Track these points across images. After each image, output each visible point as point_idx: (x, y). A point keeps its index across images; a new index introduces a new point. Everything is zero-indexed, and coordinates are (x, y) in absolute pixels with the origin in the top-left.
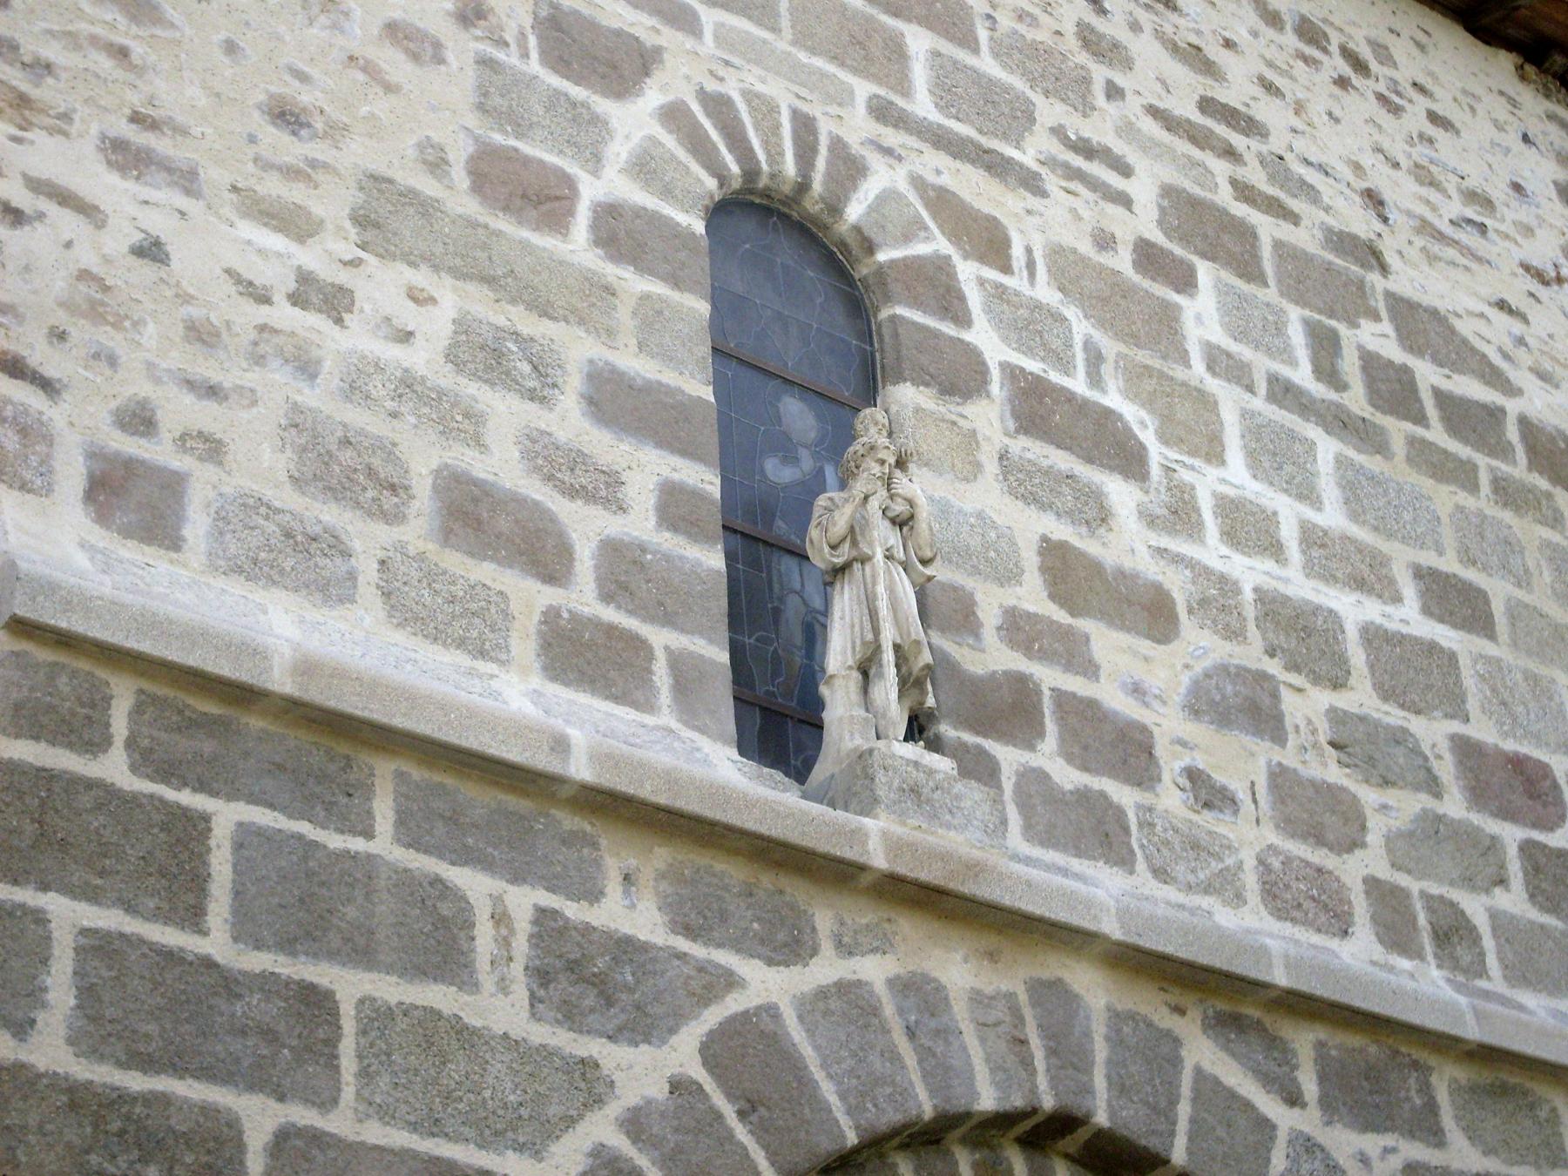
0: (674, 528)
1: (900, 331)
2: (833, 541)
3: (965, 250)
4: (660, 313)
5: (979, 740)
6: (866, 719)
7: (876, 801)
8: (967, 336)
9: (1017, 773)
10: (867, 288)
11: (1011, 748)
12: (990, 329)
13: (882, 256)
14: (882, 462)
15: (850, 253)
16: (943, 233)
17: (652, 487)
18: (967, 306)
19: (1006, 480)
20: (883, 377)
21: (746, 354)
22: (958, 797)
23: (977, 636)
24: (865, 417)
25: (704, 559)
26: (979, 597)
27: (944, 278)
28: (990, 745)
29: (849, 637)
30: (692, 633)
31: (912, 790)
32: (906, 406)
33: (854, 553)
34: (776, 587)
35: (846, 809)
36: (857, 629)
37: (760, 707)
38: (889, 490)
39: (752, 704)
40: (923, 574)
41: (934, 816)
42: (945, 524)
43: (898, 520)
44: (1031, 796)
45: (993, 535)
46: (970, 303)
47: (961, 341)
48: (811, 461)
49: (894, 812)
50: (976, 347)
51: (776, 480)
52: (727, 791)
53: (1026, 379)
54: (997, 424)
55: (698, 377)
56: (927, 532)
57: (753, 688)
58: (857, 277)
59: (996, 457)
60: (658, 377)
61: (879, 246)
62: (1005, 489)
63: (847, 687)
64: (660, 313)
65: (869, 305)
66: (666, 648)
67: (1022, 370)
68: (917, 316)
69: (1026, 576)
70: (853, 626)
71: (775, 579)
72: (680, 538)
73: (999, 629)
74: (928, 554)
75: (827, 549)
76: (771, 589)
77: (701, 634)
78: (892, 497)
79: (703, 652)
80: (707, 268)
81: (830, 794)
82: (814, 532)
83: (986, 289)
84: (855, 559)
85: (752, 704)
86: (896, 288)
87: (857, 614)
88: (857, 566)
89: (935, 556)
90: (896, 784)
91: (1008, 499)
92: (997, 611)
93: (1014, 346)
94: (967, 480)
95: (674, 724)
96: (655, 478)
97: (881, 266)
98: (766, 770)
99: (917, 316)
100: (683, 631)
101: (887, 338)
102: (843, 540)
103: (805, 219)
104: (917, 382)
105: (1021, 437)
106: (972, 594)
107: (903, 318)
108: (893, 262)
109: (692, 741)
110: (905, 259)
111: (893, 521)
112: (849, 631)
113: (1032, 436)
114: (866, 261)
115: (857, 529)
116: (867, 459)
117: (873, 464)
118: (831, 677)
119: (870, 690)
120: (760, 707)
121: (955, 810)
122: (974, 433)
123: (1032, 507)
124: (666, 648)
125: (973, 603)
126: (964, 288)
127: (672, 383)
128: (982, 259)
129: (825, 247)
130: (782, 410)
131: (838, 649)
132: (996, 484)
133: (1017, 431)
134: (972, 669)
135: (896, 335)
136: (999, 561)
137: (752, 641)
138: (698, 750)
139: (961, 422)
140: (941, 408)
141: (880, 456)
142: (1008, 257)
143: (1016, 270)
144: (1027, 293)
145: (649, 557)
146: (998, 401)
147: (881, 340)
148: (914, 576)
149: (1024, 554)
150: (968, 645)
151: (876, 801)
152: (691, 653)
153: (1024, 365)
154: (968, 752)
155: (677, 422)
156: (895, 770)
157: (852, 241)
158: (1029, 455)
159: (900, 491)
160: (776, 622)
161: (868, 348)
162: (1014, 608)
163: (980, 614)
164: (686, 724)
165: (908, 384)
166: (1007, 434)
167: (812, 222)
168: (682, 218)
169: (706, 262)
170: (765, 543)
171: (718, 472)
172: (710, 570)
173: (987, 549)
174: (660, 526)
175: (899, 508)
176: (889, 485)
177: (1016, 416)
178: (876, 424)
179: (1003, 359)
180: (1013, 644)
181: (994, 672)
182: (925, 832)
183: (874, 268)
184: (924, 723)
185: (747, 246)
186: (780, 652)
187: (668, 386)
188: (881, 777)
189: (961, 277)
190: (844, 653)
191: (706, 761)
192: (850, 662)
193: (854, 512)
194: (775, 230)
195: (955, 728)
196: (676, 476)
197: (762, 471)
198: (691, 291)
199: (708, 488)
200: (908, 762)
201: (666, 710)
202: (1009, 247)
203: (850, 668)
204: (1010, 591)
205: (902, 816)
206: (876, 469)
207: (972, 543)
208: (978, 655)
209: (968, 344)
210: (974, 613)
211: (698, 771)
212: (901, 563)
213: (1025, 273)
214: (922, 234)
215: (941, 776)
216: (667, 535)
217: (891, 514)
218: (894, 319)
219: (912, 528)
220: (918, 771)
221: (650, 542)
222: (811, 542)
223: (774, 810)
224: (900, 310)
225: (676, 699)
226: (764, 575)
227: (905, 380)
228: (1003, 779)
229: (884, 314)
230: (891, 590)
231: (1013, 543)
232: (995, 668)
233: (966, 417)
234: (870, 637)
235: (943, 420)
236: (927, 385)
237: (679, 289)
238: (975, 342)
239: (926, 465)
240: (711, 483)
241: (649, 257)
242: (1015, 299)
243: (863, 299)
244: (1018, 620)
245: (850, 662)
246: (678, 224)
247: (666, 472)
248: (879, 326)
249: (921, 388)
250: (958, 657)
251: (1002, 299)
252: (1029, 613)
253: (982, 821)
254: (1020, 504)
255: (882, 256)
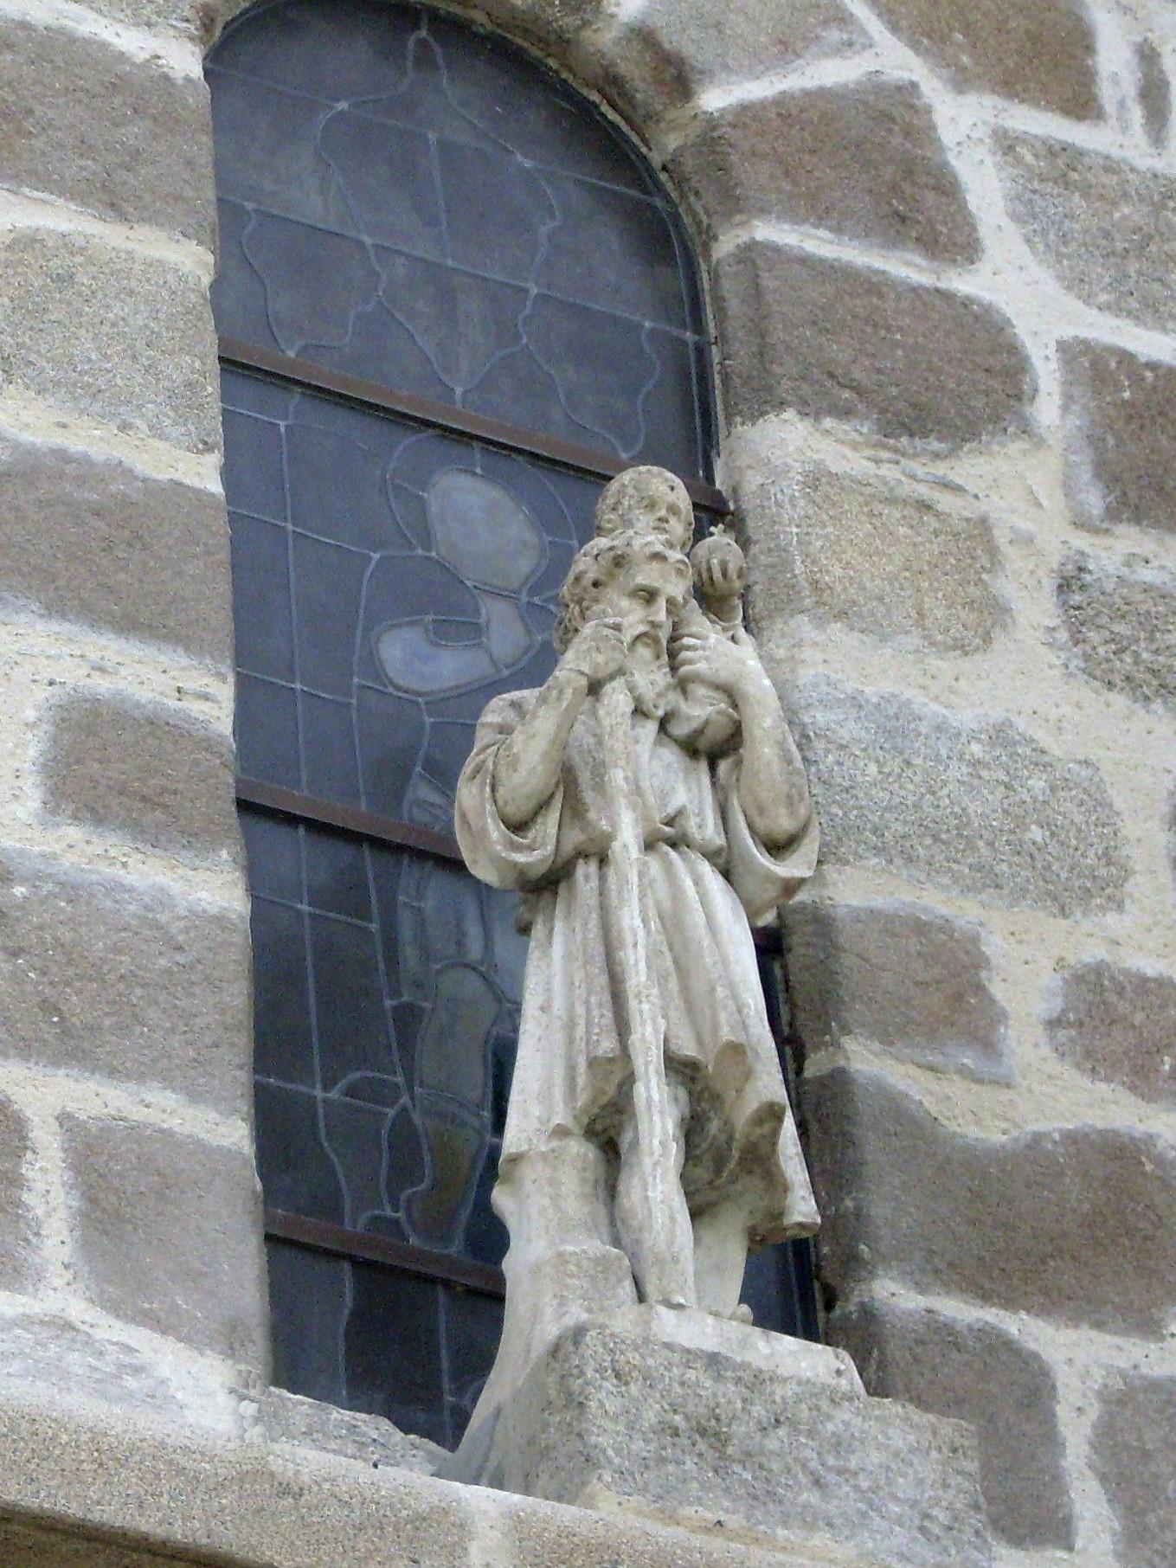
0: (94, 814)
1: (768, 281)
2: (515, 811)
3: (962, 69)
4: (65, 279)
5: (991, 1315)
6: (602, 1262)
7: (590, 1461)
8: (962, 283)
9: (1104, 1395)
10: (681, 182)
11: (1086, 1333)
12: (1029, 260)
13: (714, 99)
14: (649, 596)
15: (631, 100)
16: (894, 28)
17: (31, 714)
18: (963, 205)
19: (1077, 639)
20: (726, 405)
21: (326, 373)
22: (838, 1445)
23: (988, 1046)
24: (622, 491)
25: (176, 888)
26: (995, 945)
27: (896, 140)
28: (1019, 1326)
29: (560, 1051)
30: (141, 1078)
31: (703, 1432)
32: (779, 473)
33: (574, 837)
34: (410, 955)
35: (527, 1491)
36: (581, 1030)
37: (352, 1259)
38: (674, 669)
39: (328, 1253)
40: (769, 877)
41: (764, 1496)
42: (895, 765)
43: (703, 744)
44: (1146, 1455)
45: (1038, 784)
46: (973, 201)
47: (947, 296)
48: (518, 631)
49: (643, 1490)
50: (988, 309)
51: (414, 684)
52: (41, 1428)
53: (1137, 380)
54: (1053, 501)
55: (175, 432)
56: (776, 766)
57: (335, 1213)
58: (656, 159)
59: (1050, 584)
60: (58, 439)
61: (706, 74)
62: (1076, 663)
63: (553, 1182)
64: (65, 279)
65: (691, 230)
66: (64, 1119)
67: (1126, 357)
68: (818, 243)
69: (1137, 886)
70: (571, 1024)
71: (406, 932)
72: (112, 840)
73: (1053, 1024)
74: (783, 823)
75: (496, 832)
76: (393, 961)
77: (167, 1080)
78: (683, 686)
79: (173, 1123)
80: (204, 158)
81: (491, 1465)
82: (468, 794)
83: (1019, 161)
84: (582, 854)
85: (328, 1253)
86: (752, 175)
87: (580, 992)
88: (585, 873)
89: (805, 828)
90: (650, 1416)
91: (1086, 693)
92: (1050, 980)
93: (1103, 298)
94: (961, 647)
95: (78, 1309)
96: (42, 693)
97: (712, 122)
98: (338, 1414)
99: (818, 243)
100: (113, 1073)
101: (734, 306)
102: (543, 806)
103: (508, 29)
104: (810, 410)
105: (1121, 529)
106: (975, 940)
107: (777, 249)
108: (746, 113)
109: (130, 1350)
110: (781, 100)
111: (691, 748)
112: (559, 1037)
113: (1156, 524)
114: (672, 114)
115: (584, 778)
116: (610, 593)
117: (625, 603)
118: (515, 1159)
119: (621, 1187)
120: (352, 1259)
121: (831, 1478)
122: (984, 524)
123: (1157, 705)
124: (64, 1119)
125: (980, 962)
126: (953, 162)
127: (99, 453)
128: (1010, 86)
129: (569, 94)
130: (434, 508)
131: (535, 1086)
132: (1051, 657)
133: (1112, 515)
134: (973, 1132)
135: (756, 294)
136: (1053, 848)
137: (334, 1094)
138: (137, 1370)
139: (946, 502)
140: (888, 471)
141: (641, 580)
142: (1087, 78)
143: (1110, 108)
144: (1143, 163)
145: (19, 891)
146: (1055, 441)
147: (721, 313)
148: (750, 885)
149: (1130, 828)
150: (963, 1071)
151: (590, 1461)
152: (135, 1127)
153: (1131, 347)
154: (958, 1347)
155: (108, 549)
156: (648, 1378)
157: (633, 69)
158: (1147, 575)
159: (701, 667)
160: (407, 1042)
161: (689, 336)
162: (1099, 969)
163: (997, 989)
164: (115, 1308)
165: (790, 414)
166: (1081, 523)
167: (526, 32)
168: (132, 42)
169: (202, 149)
170: (379, 844)
171: (226, 667)
172: (198, 918)
173: (1022, 826)
174: (53, 812)
175: (700, 710)
176: (672, 655)
177: (1108, 474)
178: (651, 506)
179: (1068, 332)
180: (1095, 1062)
181: (1038, 1138)
182: (737, 1536)
183: (695, 129)
184: (833, 1282)
185: (342, 106)
186: (417, 1118)
187: (85, 460)
188: (604, 1398)
189: (948, 135)
190: (545, 1097)
191: (158, 1398)
192: (561, 1116)
193: (567, 723)
194: (424, 59)
195: (922, 1289)
196: (103, 685)
197: (374, 666)
198: (153, 218)
199: (197, 708)
200: (690, 1356)
201: (57, 1277)
202: (1090, 49)
203: (561, 1132)
204: (1086, 925)
205: (665, 1504)
206: (634, 618)
207: (974, 808)
208: (987, 1094)
209: (967, 302)
210: (979, 988)
211: (149, 1424)
212: (711, 856)
213: (1137, 114)
214: (835, 35)
215: (790, 1390)
216: (74, 833)
217: (680, 729)
218: (750, 254)
219: (739, 764)
220: (719, 1378)
221: (22, 853)
222: (463, 816)
223: (181, 1471)
224: (767, 231)
225: (87, 1247)
226: (374, 927)
227: (781, 405)
228: (1063, 1411)
229: (726, 244)
230: (672, 925)
231: (1097, 802)
232: (1041, 1127)
233: (957, 489)
234: (607, 1045)
235: (891, 501)
236: (844, 413)
237: (123, 217)
238: (987, 296)
239: (842, 615)
240: (206, 697)
241: (38, 143)
242: (1105, 179)
243: (676, 217)
244: (1112, 998)
245: (561, 1116)
246: (122, 57)
247: (74, 676)
248: (715, 278)
249: (828, 422)
250: (930, 1104)
251: (1067, 185)
252: (1144, 980)
253: (914, 1504)
254: (1119, 701)
255: (714, 99)
